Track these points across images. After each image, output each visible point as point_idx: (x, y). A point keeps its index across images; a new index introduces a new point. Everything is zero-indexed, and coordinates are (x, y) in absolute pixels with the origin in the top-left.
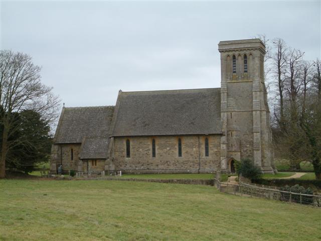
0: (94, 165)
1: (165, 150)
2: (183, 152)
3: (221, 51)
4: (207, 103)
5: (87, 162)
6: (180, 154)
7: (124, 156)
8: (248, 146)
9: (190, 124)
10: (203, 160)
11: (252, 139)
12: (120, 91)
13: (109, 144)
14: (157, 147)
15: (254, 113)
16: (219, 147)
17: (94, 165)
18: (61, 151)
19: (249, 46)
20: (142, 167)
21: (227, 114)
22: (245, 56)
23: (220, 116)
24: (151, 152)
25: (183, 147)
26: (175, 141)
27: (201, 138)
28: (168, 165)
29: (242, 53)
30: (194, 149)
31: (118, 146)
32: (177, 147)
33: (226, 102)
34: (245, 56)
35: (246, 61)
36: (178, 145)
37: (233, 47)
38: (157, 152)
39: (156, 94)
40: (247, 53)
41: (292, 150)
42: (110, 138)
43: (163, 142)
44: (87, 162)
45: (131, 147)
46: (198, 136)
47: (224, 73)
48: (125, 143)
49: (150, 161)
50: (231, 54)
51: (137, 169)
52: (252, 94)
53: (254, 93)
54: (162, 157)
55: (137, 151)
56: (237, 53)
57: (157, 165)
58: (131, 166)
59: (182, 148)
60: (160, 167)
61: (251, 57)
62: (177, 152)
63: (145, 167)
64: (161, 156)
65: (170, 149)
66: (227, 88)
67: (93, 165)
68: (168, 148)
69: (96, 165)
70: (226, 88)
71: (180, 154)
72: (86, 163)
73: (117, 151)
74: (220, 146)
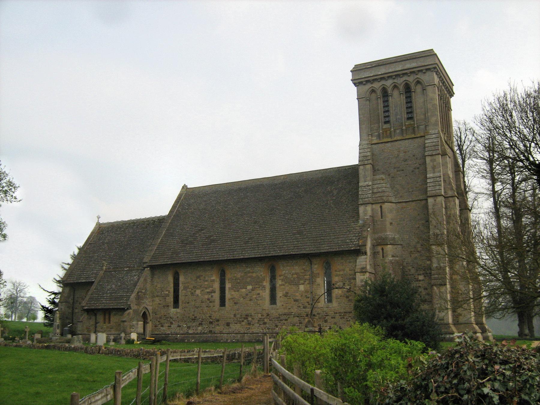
0: (107, 320)
1: (244, 290)
2: (279, 294)
3: (357, 82)
4: (335, 192)
5: (96, 315)
6: (273, 299)
7: (168, 306)
8: (421, 278)
9: (294, 234)
10: (319, 311)
11: (428, 262)
12: (185, 187)
13: (139, 279)
14: (228, 286)
15: (430, 201)
16: (352, 281)
17: (107, 320)
18: (74, 298)
19: (414, 65)
20: (200, 328)
21: (373, 210)
22: (408, 89)
23: (358, 213)
24: (217, 296)
25: (279, 282)
26: (214, 277)
27: (314, 261)
28: (249, 324)
29: (400, 81)
30: (302, 288)
31: (159, 286)
32: (267, 284)
33: (370, 183)
34: (408, 89)
35: (410, 97)
36: (268, 279)
37: (382, 71)
38: (228, 295)
39: (259, 183)
40: (411, 79)
41: (431, 160)
42: (145, 268)
43: (239, 275)
44: (96, 315)
45: (181, 286)
46: (309, 257)
47: (364, 126)
48: (171, 279)
49: (216, 316)
50: (377, 85)
51: (190, 331)
52: (425, 163)
53: (428, 159)
54: (236, 307)
55: (192, 294)
56: (389, 83)
57: (228, 324)
58: (179, 326)
59: (278, 285)
60: (235, 327)
61: (419, 88)
62: (266, 294)
63: (205, 328)
64: (235, 303)
65: (252, 290)
66: (373, 155)
67: (105, 323)
68: (250, 287)
69: (110, 323)
70: (369, 154)
71: (273, 299)
72: (94, 317)
73: (157, 296)
74: (355, 279)
